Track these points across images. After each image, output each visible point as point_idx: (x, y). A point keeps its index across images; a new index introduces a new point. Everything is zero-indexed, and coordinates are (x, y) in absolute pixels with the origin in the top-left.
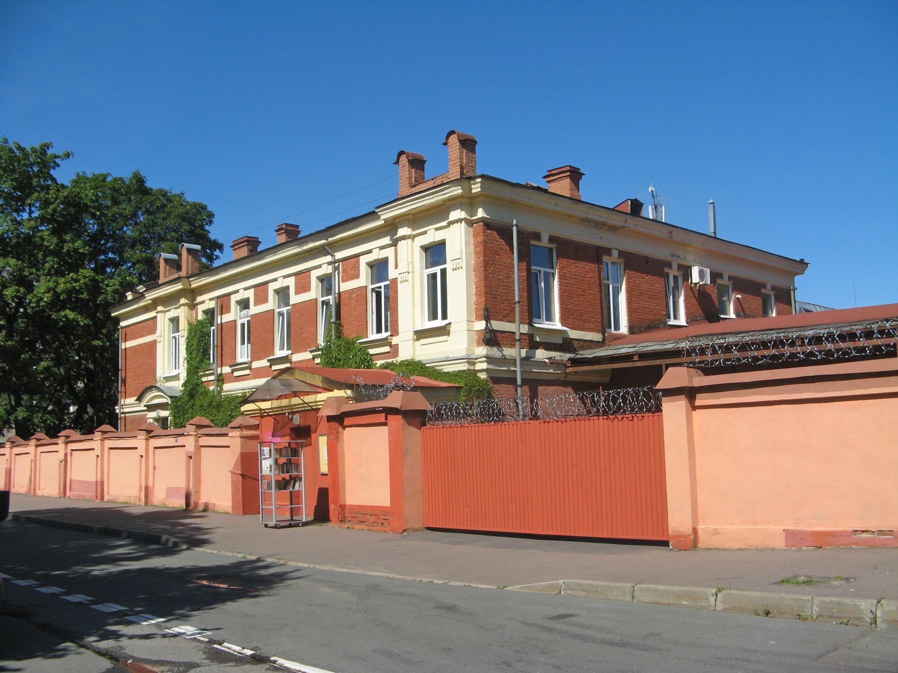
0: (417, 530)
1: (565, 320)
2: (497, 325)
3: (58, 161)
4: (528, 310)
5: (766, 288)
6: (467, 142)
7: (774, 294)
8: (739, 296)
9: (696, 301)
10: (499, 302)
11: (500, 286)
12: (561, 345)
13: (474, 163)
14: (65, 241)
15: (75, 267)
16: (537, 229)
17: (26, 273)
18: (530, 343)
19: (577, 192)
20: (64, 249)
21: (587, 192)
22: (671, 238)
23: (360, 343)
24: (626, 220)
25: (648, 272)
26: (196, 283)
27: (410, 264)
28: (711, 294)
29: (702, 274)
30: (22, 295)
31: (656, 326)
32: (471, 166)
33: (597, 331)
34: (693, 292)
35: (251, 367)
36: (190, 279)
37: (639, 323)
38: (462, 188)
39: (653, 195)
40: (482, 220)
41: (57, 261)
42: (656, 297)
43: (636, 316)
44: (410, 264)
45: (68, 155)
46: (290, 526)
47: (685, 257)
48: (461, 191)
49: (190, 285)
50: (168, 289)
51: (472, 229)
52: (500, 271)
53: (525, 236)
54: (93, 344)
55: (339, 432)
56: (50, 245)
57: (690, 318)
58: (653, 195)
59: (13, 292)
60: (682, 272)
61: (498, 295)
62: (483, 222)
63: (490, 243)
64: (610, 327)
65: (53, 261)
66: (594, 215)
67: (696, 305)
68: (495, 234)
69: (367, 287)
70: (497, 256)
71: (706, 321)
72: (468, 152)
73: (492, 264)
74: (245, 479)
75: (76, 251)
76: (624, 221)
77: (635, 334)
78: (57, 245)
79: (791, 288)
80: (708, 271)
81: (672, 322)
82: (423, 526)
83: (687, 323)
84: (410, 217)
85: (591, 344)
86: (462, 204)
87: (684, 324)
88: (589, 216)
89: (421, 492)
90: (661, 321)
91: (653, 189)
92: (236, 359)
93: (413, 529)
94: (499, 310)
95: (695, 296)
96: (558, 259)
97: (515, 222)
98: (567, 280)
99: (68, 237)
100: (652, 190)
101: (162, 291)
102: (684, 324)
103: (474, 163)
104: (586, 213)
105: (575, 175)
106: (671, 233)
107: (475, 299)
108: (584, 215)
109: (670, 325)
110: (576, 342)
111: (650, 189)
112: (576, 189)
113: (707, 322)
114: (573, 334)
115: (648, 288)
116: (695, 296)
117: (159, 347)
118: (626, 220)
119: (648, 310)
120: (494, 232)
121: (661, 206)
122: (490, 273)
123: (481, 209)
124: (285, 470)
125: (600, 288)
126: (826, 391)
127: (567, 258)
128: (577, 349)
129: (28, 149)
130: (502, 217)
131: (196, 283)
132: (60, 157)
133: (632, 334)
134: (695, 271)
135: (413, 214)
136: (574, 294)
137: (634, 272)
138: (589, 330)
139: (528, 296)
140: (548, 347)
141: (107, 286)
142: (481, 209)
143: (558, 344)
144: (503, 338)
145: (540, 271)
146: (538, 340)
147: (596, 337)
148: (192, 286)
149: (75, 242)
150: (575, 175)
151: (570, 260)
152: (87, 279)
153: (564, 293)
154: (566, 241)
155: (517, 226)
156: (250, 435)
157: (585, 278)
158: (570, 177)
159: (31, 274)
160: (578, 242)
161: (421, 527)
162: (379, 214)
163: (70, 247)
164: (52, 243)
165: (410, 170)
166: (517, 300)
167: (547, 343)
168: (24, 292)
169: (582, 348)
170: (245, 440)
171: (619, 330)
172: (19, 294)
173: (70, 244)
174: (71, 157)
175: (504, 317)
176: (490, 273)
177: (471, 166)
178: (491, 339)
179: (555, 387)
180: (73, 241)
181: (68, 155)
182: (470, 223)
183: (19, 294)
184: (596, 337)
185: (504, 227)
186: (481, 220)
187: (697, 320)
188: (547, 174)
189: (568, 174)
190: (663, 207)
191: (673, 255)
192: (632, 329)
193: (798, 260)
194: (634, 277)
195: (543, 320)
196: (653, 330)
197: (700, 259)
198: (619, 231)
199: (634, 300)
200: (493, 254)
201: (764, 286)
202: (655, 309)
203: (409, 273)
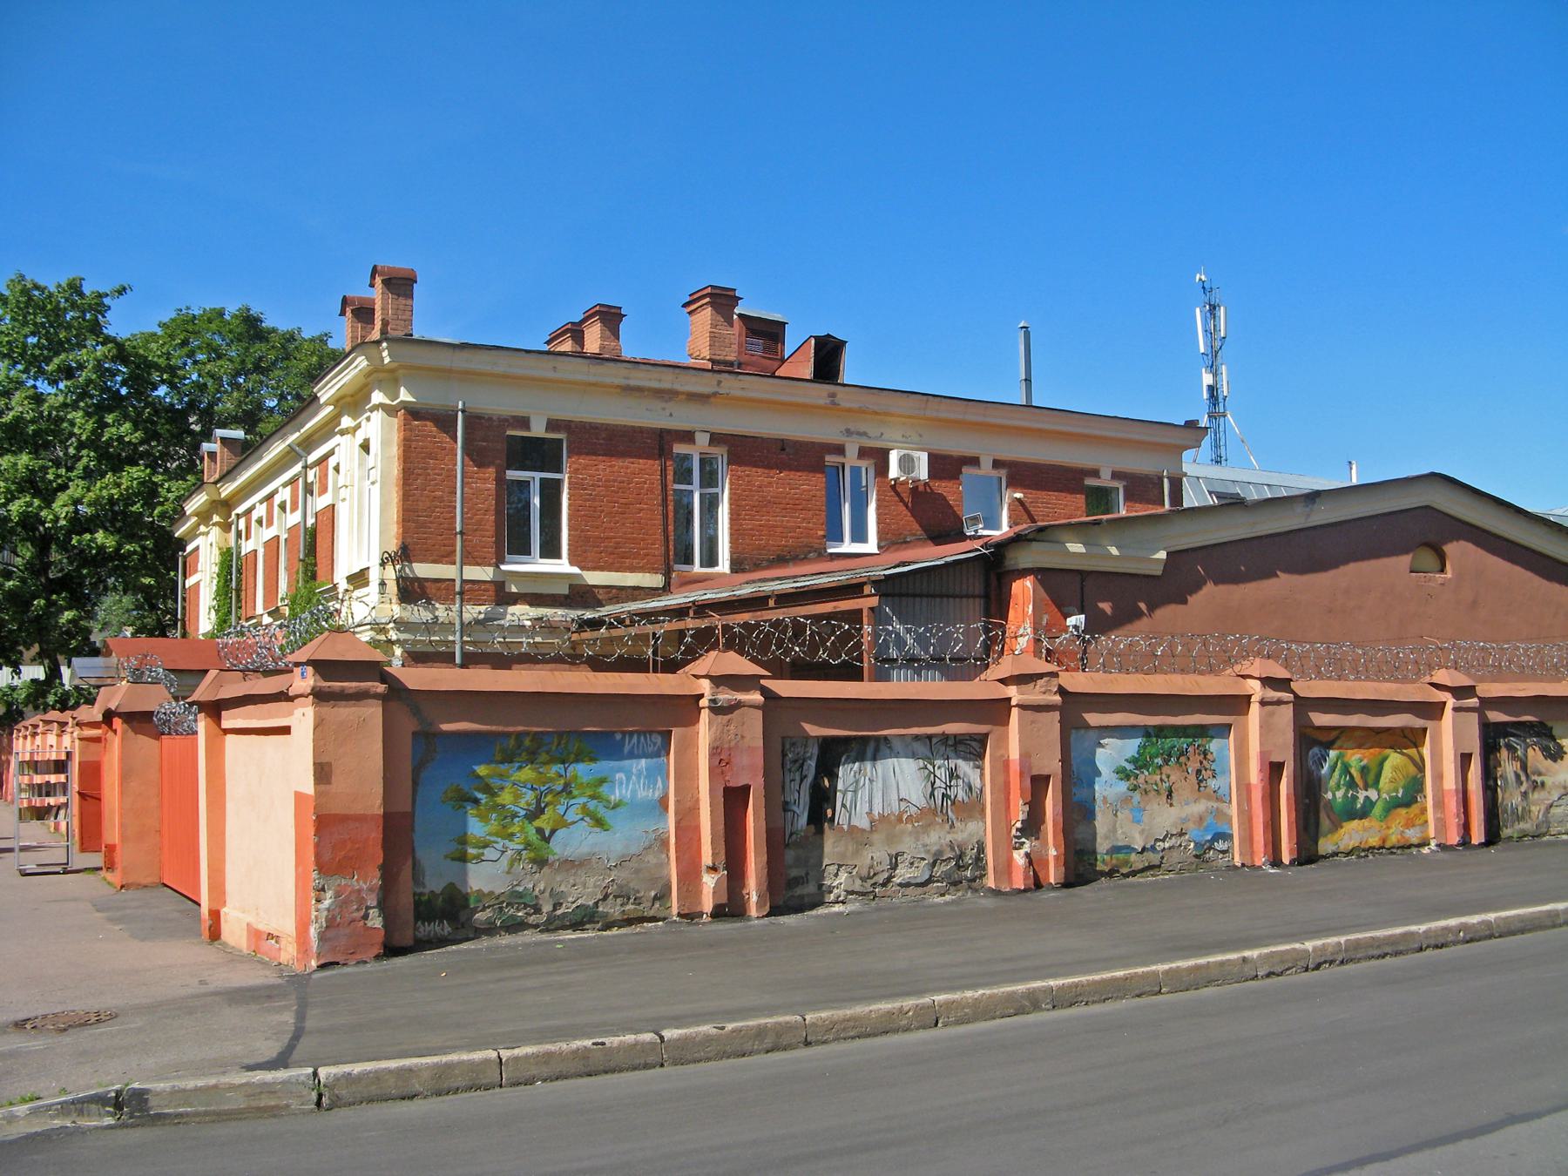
0: (146, 886)
1: (579, 555)
2: (423, 570)
3: (107, 301)
4: (495, 542)
5: (1100, 478)
6: (394, 281)
7: (1124, 486)
8: (1018, 495)
9: (904, 508)
10: (431, 533)
11: (436, 508)
12: (566, 597)
13: (408, 313)
14: (107, 425)
15: (117, 464)
16: (520, 411)
17: (50, 477)
18: (497, 595)
19: (729, 328)
20: (103, 436)
21: (631, 345)
22: (833, 403)
23: (319, 592)
24: (719, 382)
25: (781, 467)
26: (227, 490)
27: (348, 473)
28: (945, 494)
29: (907, 463)
30: (35, 511)
31: (798, 556)
32: (401, 320)
33: (654, 570)
34: (898, 494)
35: (261, 622)
36: (218, 486)
37: (755, 552)
38: (366, 358)
39: (1204, 288)
40: (405, 406)
41: (94, 457)
42: (800, 507)
43: (748, 541)
44: (348, 473)
45: (122, 291)
46: (66, 872)
47: (882, 434)
48: (366, 363)
49: (220, 494)
50: (198, 501)
51: (396, 420)
52: (437, 484)
53: (495, 423)
54: (141, 582)
55: (108, 739)
56: (82, 433)
57: (886, 539)
58: (1204, 288)
59: (22, 507)
60: (872, 461)
61: (431, 522)
62: (405, 408)
63: (417, 441)
64: (688, 560)
65: (88, 456)
66: (640, 378)
67: (906, 516)
68: (430, 427)
69: (334, 505)
70: (431, 461)
71: (930, 542)
72: (396, 297)
73: (420, 475)
74: (86, 800)
75: (120, 439)
76: (716, 383)
77: (745, 572)
78: (93, 432)
79: (1165, 474)
80: (923, 458)
81: (848, 547)
82: (158, 881)
83: (879, 547)
84: (348, 399)
85: (652, 592)
86: (381, 381)
87: (876, 551)
88: (633, 383)
89: (157, 831)
90: (812, 547)
91: (1203, 278)
92: (255, 609)
93: (139, 885)
94: (433, 546)
95: (902, 500)
96: (569, 457)
97: (460, 406)
98: (586, 489)
99: (109, 419)
100: (1200, 279)
101: (194, 505)
102: (876, 551)
103: (408, 313)
104: (625, 378)
105: (611, 317)
106: (833, 395)
107: (396, 530)
108: (623, 382)
109: (831, 554)
110: (601, 591)
111: (1198, 277)
112: (726, 324)
113: (932, 544)
114: (594, 578)
115: (781, 492)
116: (902, 500)
117: (202, 584)
118: (719, 382)
119: (779, 530)
120: (428, 423)
121: (1219, 307)
122: (416, 489)
123: (377, 391)
124: (44, 792)
125: (665, 500)
126: (270, 716)
127: (587, 454)
128: (604, 602)
129: (53, 289)
130: (437, 397)
131: (227, 490)
132: (107, 295)
133: (736, 572)
134: (894, 457)
135: (352, 396)
136: (602, 511)
137: (746, 468)
138: (632, 569)
139: (496, 521)
140: (535, 600)
141: (169, 490)
142: (377, 391)
143: (560, 595)
144: (439, 589)
145: (534, 478)
146: (514, 589)
147: (656, 580)
148: (223, 495)
149: (121, 425)
150: (611, 317)
151: (594, 458)
152: (135, 482)
153: (578, 511)
154: (588, 427)
155: (463, 411)
156: (95, 736)
157: (629, 484)
158: (602, 321)
159: (58, 476)
160: (617, 426)
161: (154, 883)
162: (318, 395)
163: (112, 433)
164: (84, 430)
165: (355, 325)
166: (458, 530)
167: (536, 594)
168: (39, 506)
169: (615, 600)
170: (86, 743)
171: (717, 564)
172: (30, 509)
173: (114, 430)
174: (128, 291)
175: (443, 556)
176: (416, 489)
177: (401, 320)
178: (410, 591)
179: (550, 665)
180: (120, 424)
181: (122, 291)
182: (390, 411)
183: (30, 509)
184: (656, 580)
185: (450, 412)
186: (402, 406)
187: (906, 542)
188: (688, 299)
189: (708, 300)
190: (1222, 308)
191: (849, 432)
192: (737, 566)
193: (1183, 424)
194: (748, 476)
195: (534, 558)
196: (791, 564)
197: (921, 436)
198: (712, 400)
199: (746, 515)
200: (424, 458)
201: (1095, 473)
202: (799, 527)
203: (347, 487)
